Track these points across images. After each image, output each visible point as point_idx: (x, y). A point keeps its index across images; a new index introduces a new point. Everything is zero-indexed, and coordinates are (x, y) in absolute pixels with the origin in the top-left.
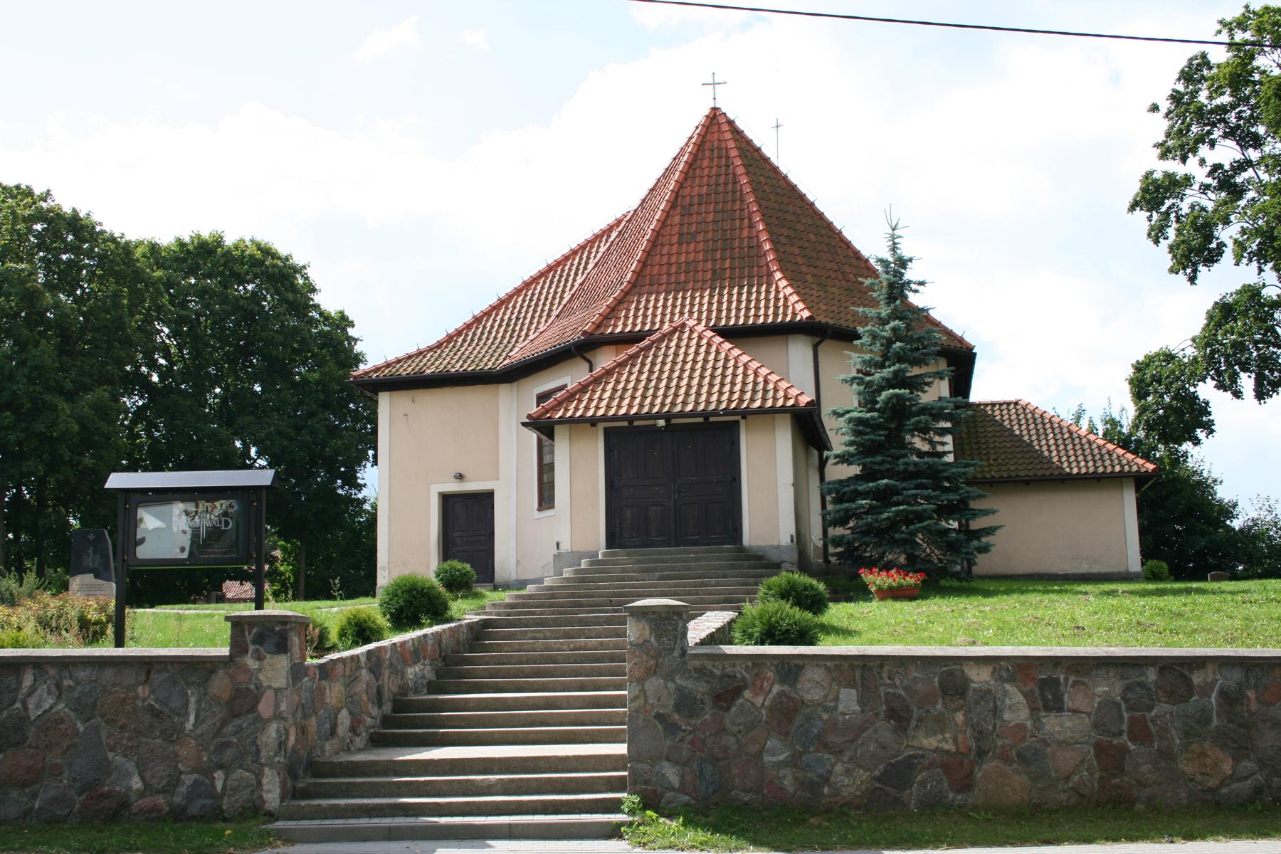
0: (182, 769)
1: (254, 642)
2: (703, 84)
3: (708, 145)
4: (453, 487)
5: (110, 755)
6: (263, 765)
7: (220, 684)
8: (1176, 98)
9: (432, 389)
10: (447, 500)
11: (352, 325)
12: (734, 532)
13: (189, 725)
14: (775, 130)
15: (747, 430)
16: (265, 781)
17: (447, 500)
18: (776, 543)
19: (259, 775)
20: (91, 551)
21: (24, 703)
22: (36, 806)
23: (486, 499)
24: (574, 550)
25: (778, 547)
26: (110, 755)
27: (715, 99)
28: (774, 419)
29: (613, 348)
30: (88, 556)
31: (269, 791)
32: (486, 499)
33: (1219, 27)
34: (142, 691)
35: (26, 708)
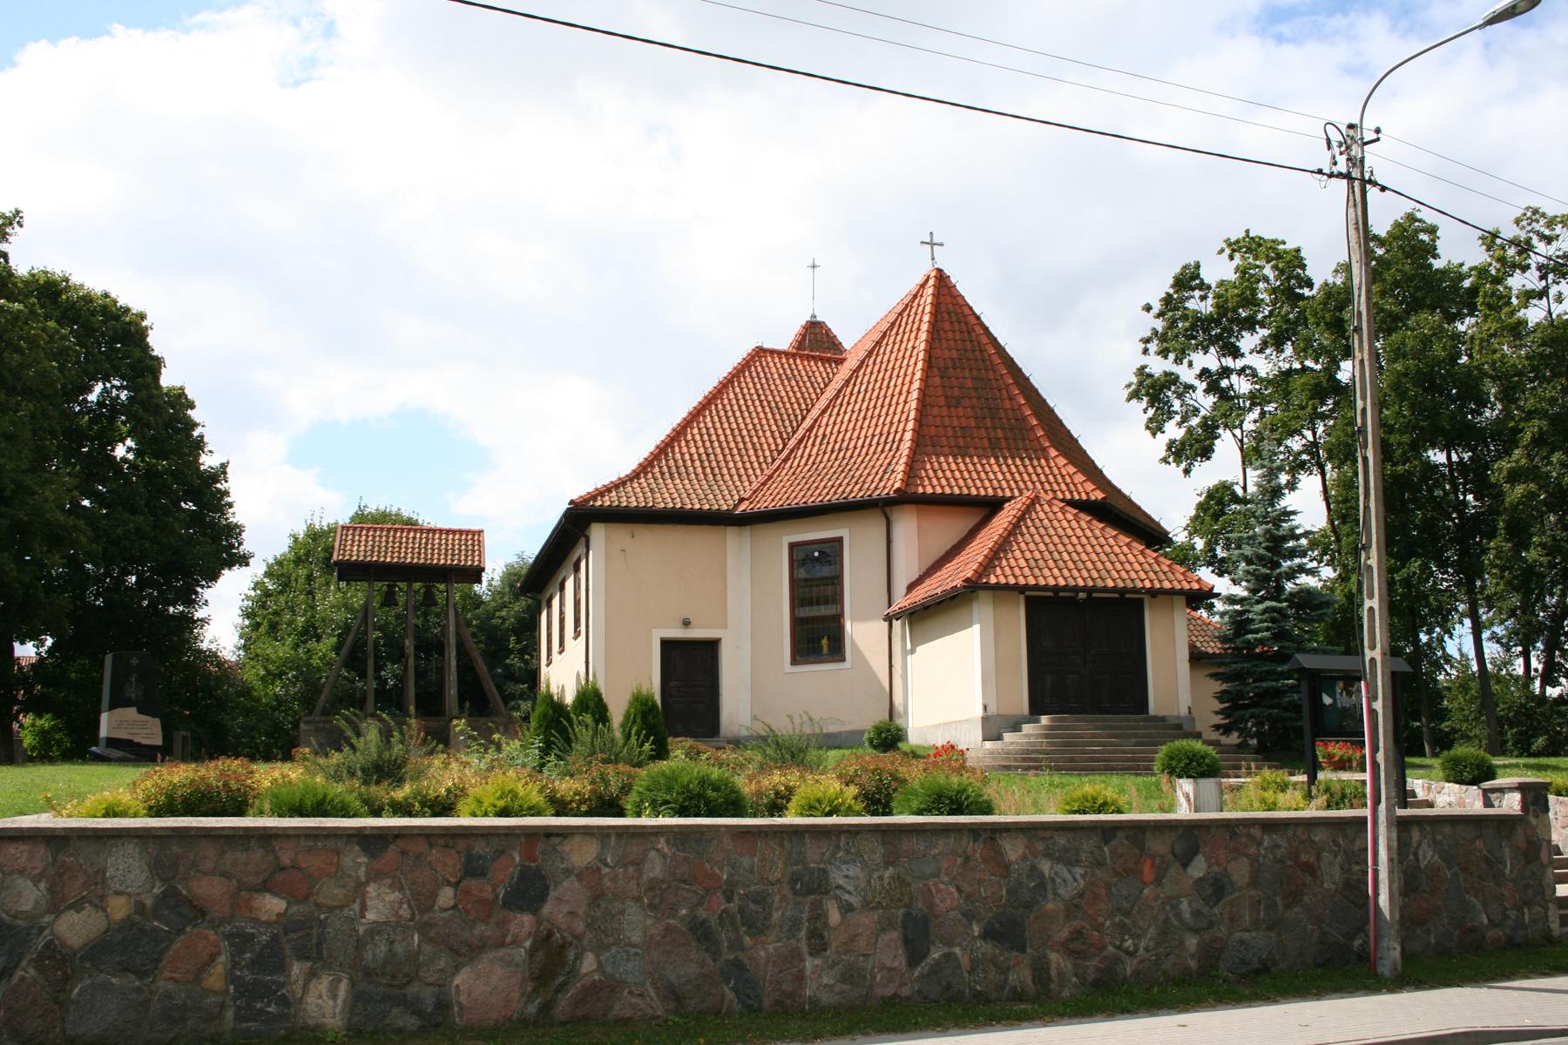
0: (1508, 906)
1: (1533, 804)
2: (922, 243)
3: (943, 308)
4: (677, 633)
5: (1467, 896)
6: (1547, 901)
7: (1520, 838)
8: (1167, 300)
9: (658, 526)
10: (668, 645)
11: (192, 406)
12: (1141, 704)
13: (1507, 871)
14: (811, 270)
15: (1150, 607)
16: (1550, 914)
17: (668, 645)
18: (1175, 713)
19: (1547, 909)
20: (133, 680)
21: (1416, 855)
22: (1433, 941)
23: (710, 648)
24: (1001, 713)
25: (1179, 717)
26: (1467, 896)
27: (933, 259)
28: (1172, 599)
29: (914, 506)
30: (131, 684)
31: (1553, 922)
32: (710, 648)
33: (1224, 245)
34: (1479, 844)
35: (1417, 860)
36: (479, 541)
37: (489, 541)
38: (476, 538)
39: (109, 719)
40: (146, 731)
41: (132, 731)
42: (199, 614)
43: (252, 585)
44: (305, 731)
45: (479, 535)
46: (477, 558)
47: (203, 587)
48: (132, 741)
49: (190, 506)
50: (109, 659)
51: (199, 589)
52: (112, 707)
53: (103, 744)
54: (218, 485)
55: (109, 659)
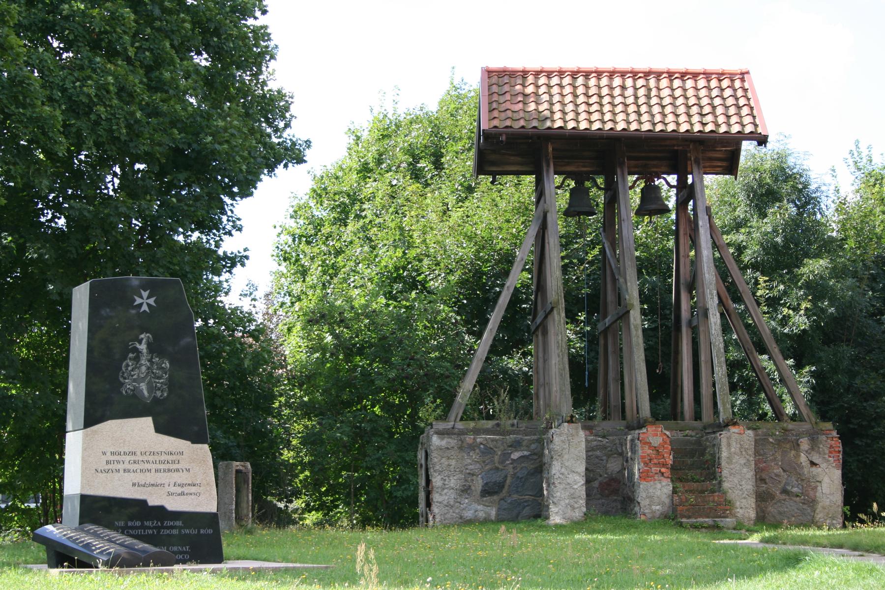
20: (143, 347)
30: (137, 359)
36: (745, 90)
37: (758, 83)
38: (737, 84)
39: (86, 448)
40: (177, 477)
41: (150, 478)
42: (229, 246)
43: (291, 210)
44: (440, 449)
45: (743, 80)
46: (747, 120)
47: (232, 196)
48: (144, 502)
49: (203, 61)
50: (81, 295)
51: (226, 199)
52: (91, 420)
53: (71, 510)
54: (250, 22)
55: (81, 295)
